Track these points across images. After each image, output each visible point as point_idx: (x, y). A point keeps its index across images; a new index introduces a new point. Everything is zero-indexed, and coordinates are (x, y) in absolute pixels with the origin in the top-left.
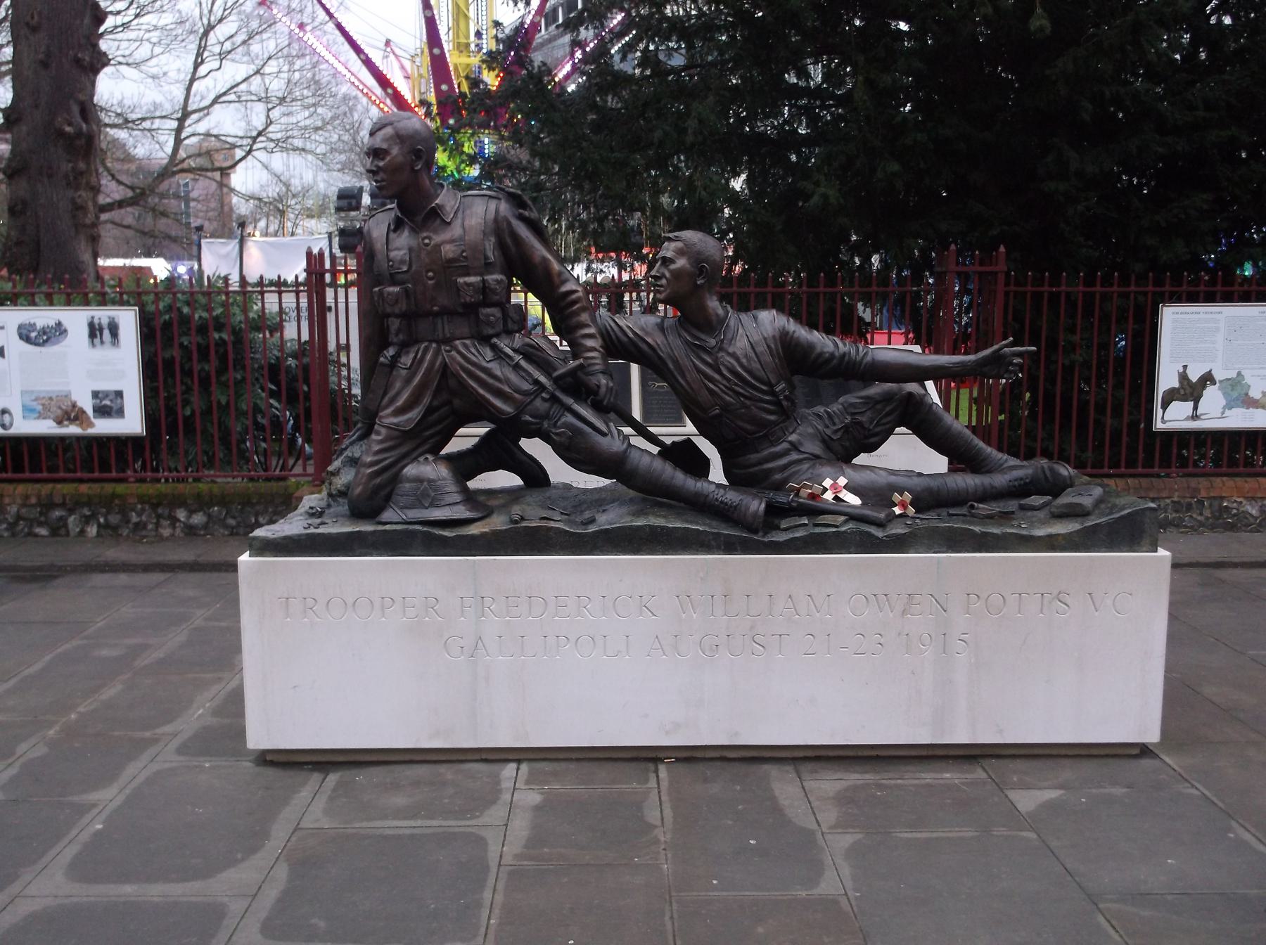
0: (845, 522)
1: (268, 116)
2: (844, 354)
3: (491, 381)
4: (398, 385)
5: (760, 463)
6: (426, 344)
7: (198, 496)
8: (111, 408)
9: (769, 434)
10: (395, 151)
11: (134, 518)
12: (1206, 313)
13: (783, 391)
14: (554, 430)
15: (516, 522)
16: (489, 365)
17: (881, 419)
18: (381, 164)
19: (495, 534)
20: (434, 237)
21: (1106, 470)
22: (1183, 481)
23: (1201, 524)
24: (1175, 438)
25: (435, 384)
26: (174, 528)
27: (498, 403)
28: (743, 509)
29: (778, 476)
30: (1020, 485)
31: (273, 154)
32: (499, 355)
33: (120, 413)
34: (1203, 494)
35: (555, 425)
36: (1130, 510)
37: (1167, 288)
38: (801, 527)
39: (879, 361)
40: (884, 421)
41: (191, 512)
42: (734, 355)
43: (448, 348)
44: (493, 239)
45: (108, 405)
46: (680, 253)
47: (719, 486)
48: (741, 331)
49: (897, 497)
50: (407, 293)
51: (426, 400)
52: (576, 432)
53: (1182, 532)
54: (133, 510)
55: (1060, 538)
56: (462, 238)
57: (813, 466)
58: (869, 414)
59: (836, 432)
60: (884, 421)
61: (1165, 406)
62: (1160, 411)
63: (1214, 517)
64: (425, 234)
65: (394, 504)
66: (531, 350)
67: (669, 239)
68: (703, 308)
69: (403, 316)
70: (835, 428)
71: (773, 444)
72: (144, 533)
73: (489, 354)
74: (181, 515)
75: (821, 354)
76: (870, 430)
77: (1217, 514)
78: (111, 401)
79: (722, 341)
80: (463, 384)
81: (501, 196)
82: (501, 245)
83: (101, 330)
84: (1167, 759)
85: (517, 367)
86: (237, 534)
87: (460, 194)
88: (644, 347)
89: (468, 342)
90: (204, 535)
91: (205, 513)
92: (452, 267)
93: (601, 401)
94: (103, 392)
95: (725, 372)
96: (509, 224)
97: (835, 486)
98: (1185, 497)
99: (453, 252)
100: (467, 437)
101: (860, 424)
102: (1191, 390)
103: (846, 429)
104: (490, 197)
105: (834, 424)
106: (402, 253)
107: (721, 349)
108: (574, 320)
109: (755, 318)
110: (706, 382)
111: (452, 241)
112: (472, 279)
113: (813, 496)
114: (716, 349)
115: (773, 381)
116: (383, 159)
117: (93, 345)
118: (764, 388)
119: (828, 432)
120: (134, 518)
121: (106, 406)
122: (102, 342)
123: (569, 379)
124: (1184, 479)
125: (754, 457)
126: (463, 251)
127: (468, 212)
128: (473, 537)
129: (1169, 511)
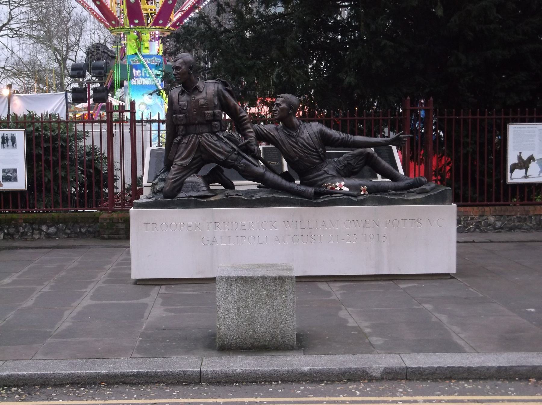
0: (343, 195)
1: (10, 14)
2: (343, 138)
3: (217, 148)
4: (182, 150)
5: (313, 178)
6: (192, 135)
7: (53, 219)
8: (11, 177)
9: (316, 167)
10: (183, 67)
11: (22, 230)
12: (529, 128)
13: (321, 151)
14: (239, 165)
15: (227, 196)
16: (215, 142)
17: (358, 162)
18: (178, 72)
19: (220, 200)
20: (196, 97)
21: (485, 203)
22: (522, 208)
23: (532, 228)
24: (518, 187)
25: (196, 149)
26: (41, 234)
27: (219, 155)
28: (307, 191)
29: (320, 183)
30: (409, 185)
31: (12, 39)
32: (219, 139)
33: (15, 179)
34: (531, 213)
35: (239, 163)
36: (441, 190)
37: (511, 116)
38: (328, 198)
39: (356, 140)
40: (360, 163)
41: (49, 227)
42: (303, 138)
43: (201, 136)
44: (217, 97)
45: (10, 176)
46: (283, 102)
47: (298, 185)
48: (305, 130)
49: (362, 188)
50: (186, 116)
51: (193, 155)
52: (247, 165)
53: (523, 232)
54: (21, 226)
55: (418, 200)
56: (206, 97)
57: (332, 179)
58: (353, 160)
59: (341, 167)
60: (360, 163)
61: (512, 172)
62: (509, 174)
63: (537, 224)
64: (192, 96)
65: (183, 191)
66: (230, 137)
67: (279, 97)
68: (291, 121)
69: (184, 125)
70: (341, 165)
71: (318, 171)
72: (26, 237)
73: (215, 138)
74: (44, 228)
75: (335, 138)
76: (354, 166)
77: (538, 223)
78: (11, 174)
79: (299, 133)
80: (206, 149)
81: (219, 82)
82: (220, 100)
83: (7, 140)
84: (459, 279)
85: (226, 143)
86: (71, 237)
87: (204, 82)
88: (270, 136)
89: (207, 134)
90: (55, 238)
91: (55, 227)
92: (202, 108)
93: (256, 155)
94: (7, 169)
95: (300, 145)
96: (222, 92)
97: (340, 185)
98: (523, 215)
99: (203, 102)
100: (206, 169)
101: (350, 164)
102: (523, 164)
103: (345, 166)
104: (216, 83)
105: (341, 164)
106: (184, 102)
107: (298, 136)
108: (245, 126)
109: (311, 125)
110: (293, 148)
111: (203, 98)
112: (210, 112)
113: (332, 188)
114: (296, 136)
115: (317, 148)
116: (179, 70)
117: (4, 147)
118: (314, 150)
119: (339, 167)
120: (22, 230)
121: (8, 176)
122: (8, 146)
123: (244, 147)
124: (522, 207)
125: (311, 176)
126: (206, 102)
127: (208, 88)
128: (212, 201)
129: (516, 221)
